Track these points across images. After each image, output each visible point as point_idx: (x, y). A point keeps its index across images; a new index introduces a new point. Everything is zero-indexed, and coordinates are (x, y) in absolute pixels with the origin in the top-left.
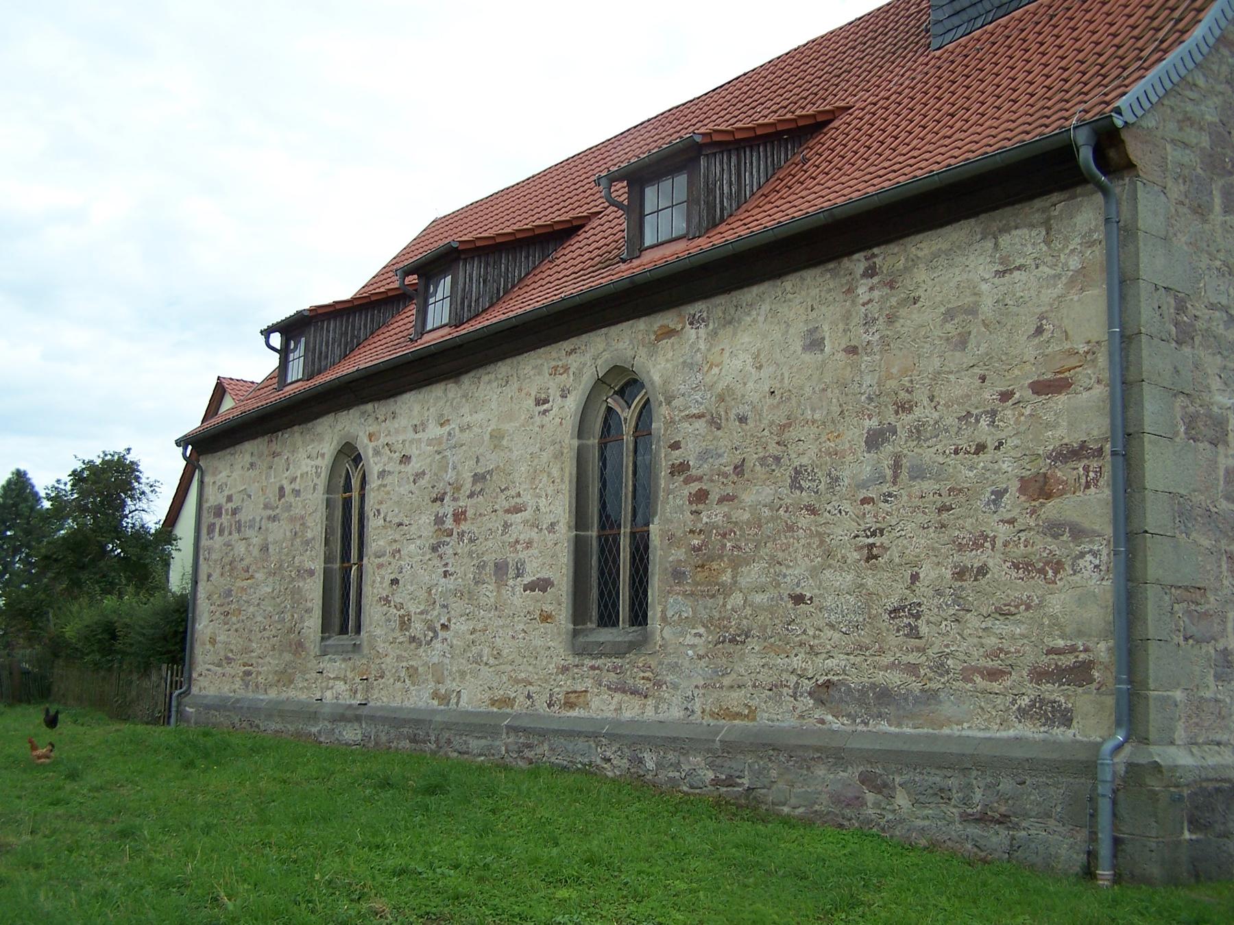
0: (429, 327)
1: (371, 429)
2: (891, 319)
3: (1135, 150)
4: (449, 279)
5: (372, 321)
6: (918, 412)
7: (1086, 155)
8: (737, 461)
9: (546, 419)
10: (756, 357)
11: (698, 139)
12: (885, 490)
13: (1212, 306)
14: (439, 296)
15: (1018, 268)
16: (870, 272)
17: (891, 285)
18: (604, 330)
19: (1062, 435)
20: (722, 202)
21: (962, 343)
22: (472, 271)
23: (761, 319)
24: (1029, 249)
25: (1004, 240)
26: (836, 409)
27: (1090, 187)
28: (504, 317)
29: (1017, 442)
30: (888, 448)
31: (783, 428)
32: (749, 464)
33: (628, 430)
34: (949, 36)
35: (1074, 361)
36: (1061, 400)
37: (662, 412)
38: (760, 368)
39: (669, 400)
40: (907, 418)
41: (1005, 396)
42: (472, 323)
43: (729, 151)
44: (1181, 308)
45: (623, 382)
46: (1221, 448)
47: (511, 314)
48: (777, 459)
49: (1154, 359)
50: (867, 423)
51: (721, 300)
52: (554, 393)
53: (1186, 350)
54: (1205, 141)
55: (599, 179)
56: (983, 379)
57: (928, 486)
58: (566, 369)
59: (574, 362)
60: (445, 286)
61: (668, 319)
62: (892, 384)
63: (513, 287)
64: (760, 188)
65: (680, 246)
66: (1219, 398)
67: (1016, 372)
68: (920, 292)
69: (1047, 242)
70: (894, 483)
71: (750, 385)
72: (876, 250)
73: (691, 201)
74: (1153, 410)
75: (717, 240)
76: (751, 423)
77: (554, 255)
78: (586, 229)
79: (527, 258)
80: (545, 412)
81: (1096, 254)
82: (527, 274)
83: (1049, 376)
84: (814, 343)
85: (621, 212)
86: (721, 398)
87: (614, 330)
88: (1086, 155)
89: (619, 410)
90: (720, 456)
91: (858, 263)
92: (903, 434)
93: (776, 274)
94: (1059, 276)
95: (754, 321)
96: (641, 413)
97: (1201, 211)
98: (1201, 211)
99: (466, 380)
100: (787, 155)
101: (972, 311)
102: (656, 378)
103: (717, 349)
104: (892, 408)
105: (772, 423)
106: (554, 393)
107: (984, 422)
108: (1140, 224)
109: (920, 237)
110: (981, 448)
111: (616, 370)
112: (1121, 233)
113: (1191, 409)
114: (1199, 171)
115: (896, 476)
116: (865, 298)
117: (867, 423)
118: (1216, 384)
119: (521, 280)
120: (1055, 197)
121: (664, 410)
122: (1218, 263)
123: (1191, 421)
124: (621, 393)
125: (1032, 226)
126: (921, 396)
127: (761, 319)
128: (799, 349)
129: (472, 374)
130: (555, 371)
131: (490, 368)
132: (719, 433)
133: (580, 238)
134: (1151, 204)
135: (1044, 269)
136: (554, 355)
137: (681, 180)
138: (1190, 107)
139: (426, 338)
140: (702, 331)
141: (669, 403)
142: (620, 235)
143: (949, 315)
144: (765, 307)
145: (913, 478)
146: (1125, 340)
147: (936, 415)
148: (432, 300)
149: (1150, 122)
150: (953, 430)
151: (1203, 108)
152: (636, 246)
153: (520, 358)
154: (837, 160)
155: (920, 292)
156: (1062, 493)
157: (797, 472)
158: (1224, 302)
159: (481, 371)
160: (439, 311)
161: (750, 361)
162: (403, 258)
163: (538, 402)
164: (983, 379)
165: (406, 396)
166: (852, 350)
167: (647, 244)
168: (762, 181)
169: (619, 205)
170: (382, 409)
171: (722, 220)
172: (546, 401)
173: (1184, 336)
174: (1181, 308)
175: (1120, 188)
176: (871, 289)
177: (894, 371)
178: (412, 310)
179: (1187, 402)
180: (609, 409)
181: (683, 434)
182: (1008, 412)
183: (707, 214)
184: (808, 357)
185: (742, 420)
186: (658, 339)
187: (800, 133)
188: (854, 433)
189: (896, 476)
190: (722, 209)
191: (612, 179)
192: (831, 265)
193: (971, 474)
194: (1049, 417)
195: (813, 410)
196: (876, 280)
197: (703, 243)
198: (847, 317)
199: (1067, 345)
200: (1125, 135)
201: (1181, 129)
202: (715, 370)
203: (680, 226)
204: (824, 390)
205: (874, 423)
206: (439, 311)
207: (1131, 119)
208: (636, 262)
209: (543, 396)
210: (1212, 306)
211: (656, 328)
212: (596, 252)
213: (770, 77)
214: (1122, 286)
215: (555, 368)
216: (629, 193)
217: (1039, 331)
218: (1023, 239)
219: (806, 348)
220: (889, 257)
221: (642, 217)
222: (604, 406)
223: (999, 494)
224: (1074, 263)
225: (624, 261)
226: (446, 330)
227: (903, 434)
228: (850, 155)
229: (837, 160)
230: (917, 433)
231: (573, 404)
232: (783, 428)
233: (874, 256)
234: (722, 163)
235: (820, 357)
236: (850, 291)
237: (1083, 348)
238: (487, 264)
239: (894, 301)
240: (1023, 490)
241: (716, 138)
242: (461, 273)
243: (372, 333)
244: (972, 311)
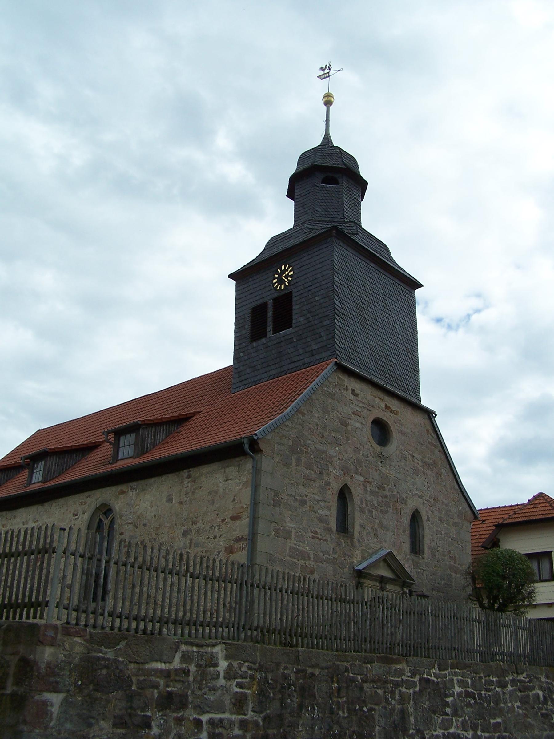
0: (33, 482)
1: (4, 522)
2: (193, 493)
3: (262, 446)
4: (43, 462)
5: (7, 476)
6: (198, 525)
7: (246, 447)
8: (142, 540)
9: (76, 522)
10: (151, 503)
11: (140, 423)
12: (187, 551)
13: (289, 495)
14: (38, 469)
15: (230, 479)
16: (189, 477)
17: (194, 481)
18: (101, 490)
19: (238, 533)
20: (147, 445)
21: (213, 502)
22: (53, 461)
23: (154, 490)
24: (233, 474)
25: (227, 470)
26: (174, 523)
27: (248, 456)
28: (63, 481)
29: (225, 535)
30: (189, 537)
31: (157, 529)
32: (145, 541)
33: (106, 528)
34: (237, 389)
35: (241, 510)
36: (238, 522)
37: (118, 521)
38: (152, 507)
39: (121, 517)
40: (195, 527)
41: (223, 520)
42: (51, 482)
43: (152, 427)
44: (276, 495)
45: (106, 510)
46: (288, 540)
47: (66, 480)
48: (155, 539)
49: (264, 511)
50: (183, 528)
51: (142, 482)
52: (80, 512)
53: (277, 509)
54: (290, 443)
55: (104, 432)
56: (218, 515)
57: (199, 549)
58: (85, 503)
59: (89, 500)
60: (41, 466)
61: (123, 487)
62: (191, 515)
63: (69, 468)
64: (163, 440)
65: (130, 461)
66: (290, 525)
67: (227, 513)
68: (203, 485)
69: (238, 472)
70: (190, 548)
71: (148, 513)
72: (191, 469)
73: (136, 444)
74: (261, 526)
75: (145, 460)
76: (147, 527)
77: (87, 456)
78: (101, 447)
79: (76, 456)
80: (76, 519)
81: (250, 477)
82: (76, 463)
83: (235, 515)
84: (170, 500)
85: (111, 446)
86: (139, 517)
87: (104, 490)
88: (246, 447)
89: (103, 520)
90: (137, 538)
91: (185, 473)
92: (193, 532)
93: (160, 474)
94: (240, 483)
95: (152, 490)
96: (111, 522)
97: (287, 465)
98: (287, 465)
99: (46, 505)
100: (174, 428)
101: (216, 492)
102: (117, 509)
103: (138, 499)
104: (191, 523)
105: (154, 527)
106: (80, 512)
107: (216, 529)
108: (262, 469)
109: (204, 466)
110: (215, 537)
111: (104, 505)
112: (257, 471)
113: (277, 527)
114: (287, 452)
115: (190, 546)
116: (186, 485)
117: (183, 528)
118: (288, 520)
119: (73, 465)
120: (242, 458)
121: (119, 521)
122: (292, 482)
123: (277, 531)
124: (105, 513)
125: (235, 466)
126: (200, 519)
127: (154, 490)
128: (165, 501)
129: (49, 502)
130: (81, 504)
131: (57, 501)
132: (137, 530)
133: (98, 450)
134: (266, 463)
135: (237, 480)
136: (81, 497)
137: (133, 436)
138: (285, 432)
139: (31, 486)
140: (134, 493)
141: (121, 518)
142: (110, 453)
143: (210, 493)
144: (156, 486)
145: (195, 547)
146: (255, 504)
147: (203, 526)
148: (35, 471)
149: (269, 437)
150: (208, 531)
151: (291, 433)
152: (115, 458)
153: (68, 497)
154: (270, 397)
155: (203, 485)
156: (236, 552)
157: (161, 544)
158: (294, 494)
159: (53, 501)
160: (38, 476)
161: (149, 504)
162: (22, 447)
163: (75, 515)
164: (218, 515)
165: (21, 510)
166: (181, 503)
167: (120, 458)
168: (164, 438)
169: (111, 443)
170: (9, 514)
171: (147, 452)
172: (77, 515)
173: (276, 504)
174: (276, 495)
175: (257, 457)
176: (188, 483)
177: (193, 510)
178: (26, 473)
179: (276, 525)
180: (100, 520)
181: (125, 530)
182: (224, 526)
183: (141, 450)
184: (167, 504)
185: (145, 525)
186: (120, 494)
187: (180, 421)
188: (179, 532)
189: (190, 546)
190: (147, 448)
191: (109, 432)
192: (177, 473)
193: (211, 546)
194: (234, 528)
195: (167, 522)
196: (190, 479)
197: (138, 461)
198: (180, 491)
199: (241, 505)
200: (259, 441)
201: (281, 439)
202: (137, 507)
203: (131, 454)
204: (171, 516)
205: (185, 528)
206: (38, 476)
207: (260, 436)
208: (115, 465)
209: (76, 513)
210: (289, 495)
211: (119, 490)
212: (103, 458)
213: (182, 390)
214: (256, 488)
215: (82, 502)
216: (115, 438)
217: (234, 500)
218: (232, 471)
219: (167, 501)
220: (195, 472)
221: (118, 447)
222: (98, 518)
223: (219, 552)
224: (245, 480)
225: (110, 464)
226: (40, 484)
227: (193, 532)
228: (275, 395)
229: (270, 397)
230: (198, 532)
231: (87, 516)
232: (157, 529)
233: (190, 471)
234: (148, 431)
235: (171, 505)
236: (182, 482)
237: (245, 506)
238: (59, 458)
239: (194, 487)
240: (225, 551)
241: (147, 422)
242: (48, 462)
243: (7, 481)
244: (216, 492)
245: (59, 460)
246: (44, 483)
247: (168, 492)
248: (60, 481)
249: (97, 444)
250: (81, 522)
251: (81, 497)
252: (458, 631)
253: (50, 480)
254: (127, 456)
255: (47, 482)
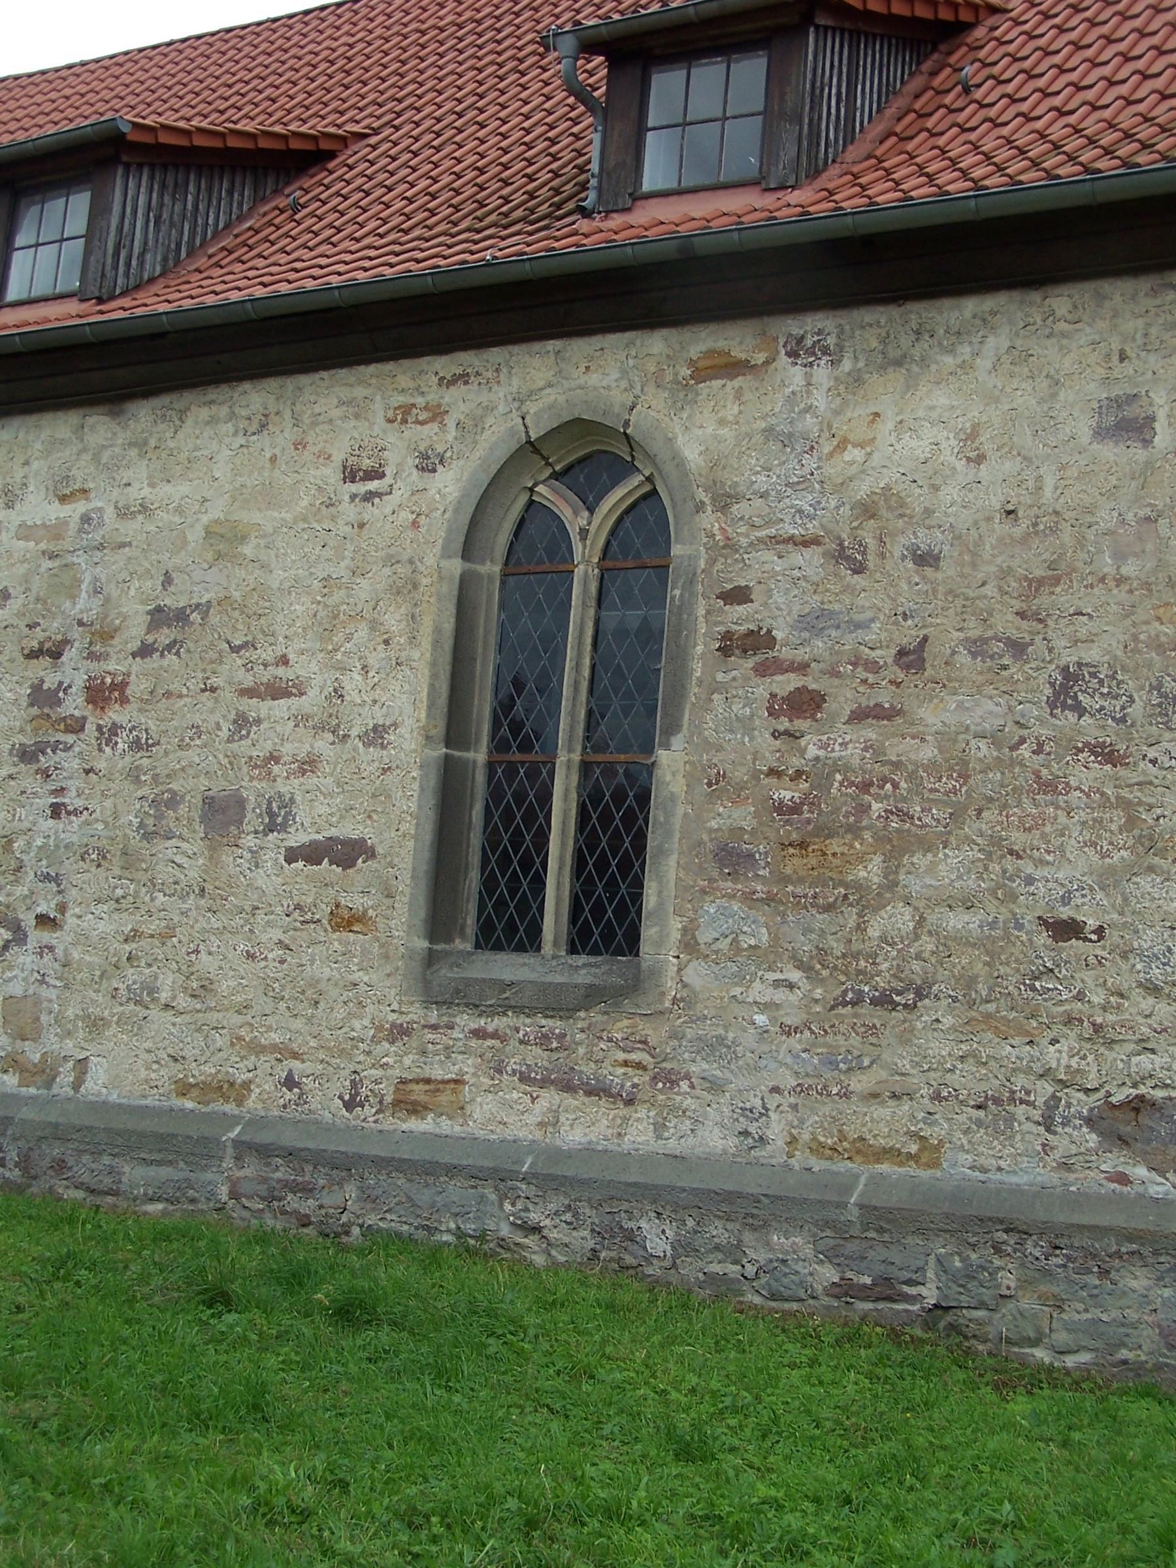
18: (552, 345)
22: (133, 194)
31: (1036, 585)
39: (724, 501)
48: (1018, 648)
59: (461, 402)
76: (948, 569)
87: (580, 348)
127: (984, 363)
128: (1085, 433)
129: (165, 399)
130: (403, 415)
131: (213, 393)
137: (751, 71)
139: (643, 215)
153: (304, 380)
172: (375, 474)
184: (1108, 452)
202: (854, 454)
208: (617, 221)
215: (407, 409)
219: (1100, 434)
231: (451, 486)
235: (1140, 454)
238: (163, 186)
245: (161, 196)
246: (100, 301)
247: (1106, 381)
248: (157, 303)
249: (324, 145)
250: (406, 516)
251: (404, 381)
252: (231, 763)
253: (123, 294)
254: (49, 291)
255: (112, 297)
